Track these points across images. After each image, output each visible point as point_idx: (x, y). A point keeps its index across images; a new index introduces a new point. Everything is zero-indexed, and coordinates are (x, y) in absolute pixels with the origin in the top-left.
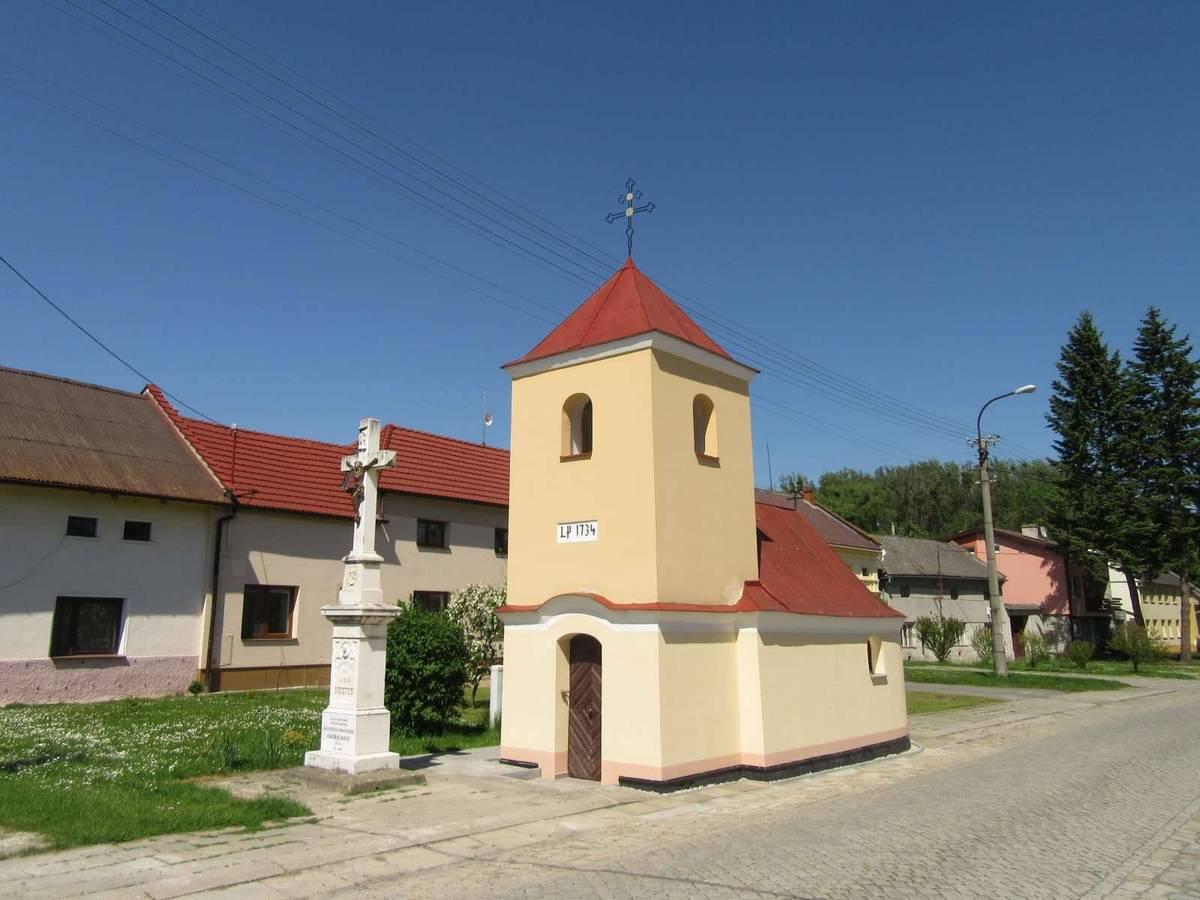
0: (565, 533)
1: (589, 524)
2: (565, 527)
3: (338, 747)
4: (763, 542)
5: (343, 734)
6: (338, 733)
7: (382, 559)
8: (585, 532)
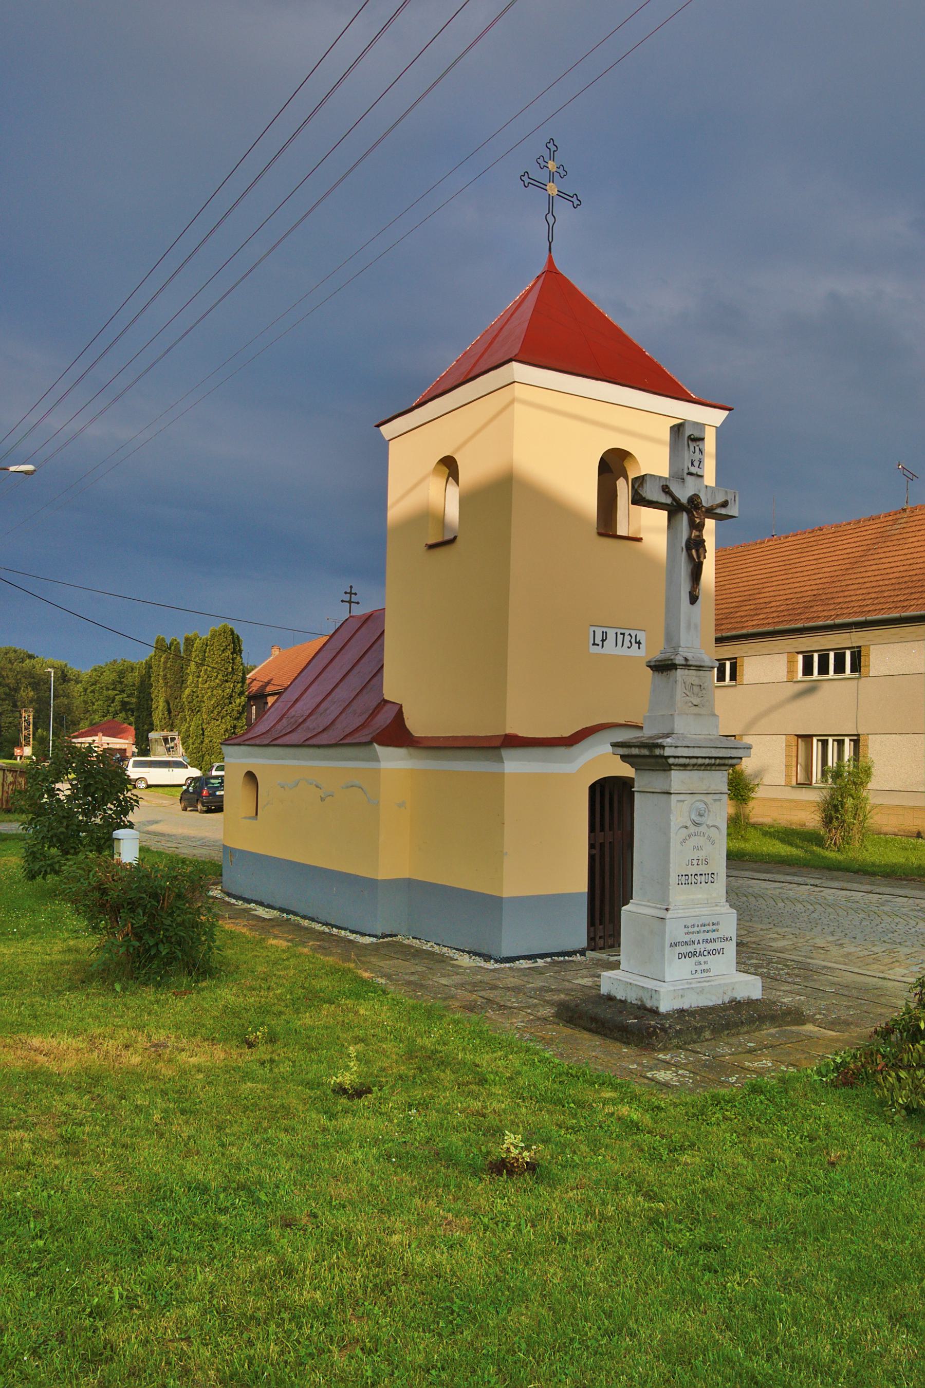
0: (598, 641)
3: (699, 968)
5: (710, 946)
6: (699, 948)
8: (627, 643)
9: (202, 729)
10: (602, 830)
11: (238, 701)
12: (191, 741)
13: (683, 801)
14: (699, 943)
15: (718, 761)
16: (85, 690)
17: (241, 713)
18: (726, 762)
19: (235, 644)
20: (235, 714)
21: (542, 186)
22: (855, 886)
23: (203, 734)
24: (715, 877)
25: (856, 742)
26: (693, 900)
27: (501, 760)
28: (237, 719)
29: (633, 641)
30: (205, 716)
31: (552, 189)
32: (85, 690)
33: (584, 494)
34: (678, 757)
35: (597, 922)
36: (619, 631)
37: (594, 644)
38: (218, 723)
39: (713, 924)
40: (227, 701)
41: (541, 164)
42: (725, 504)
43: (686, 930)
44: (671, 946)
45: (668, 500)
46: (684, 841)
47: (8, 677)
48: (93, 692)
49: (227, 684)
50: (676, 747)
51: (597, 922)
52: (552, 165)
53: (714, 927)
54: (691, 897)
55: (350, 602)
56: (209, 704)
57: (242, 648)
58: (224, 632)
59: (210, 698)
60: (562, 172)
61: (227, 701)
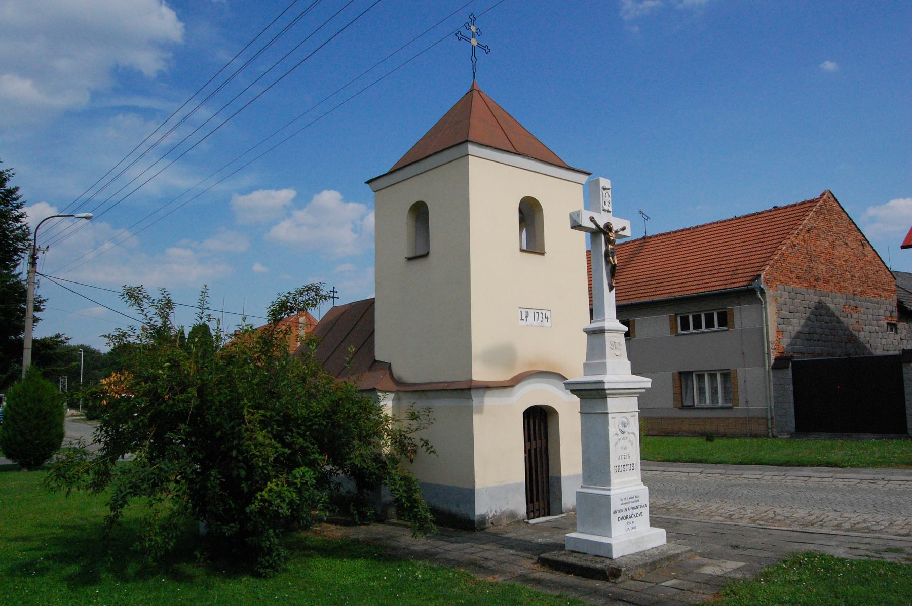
0: (524, 318)
2: (524, 311)
3: (630, 526)
5: (635, 512)
6: (629, 513)
8: (540, 319)
10: (535, 440)
22: (670, 469)
25: (726, 375)
27: (470, 398)
31: (474, 42)
41: (467, 26)
42: (624, 229)
45: (594, 227)
52: (473, 29)
55: (333, 297)
60: (479, 33)
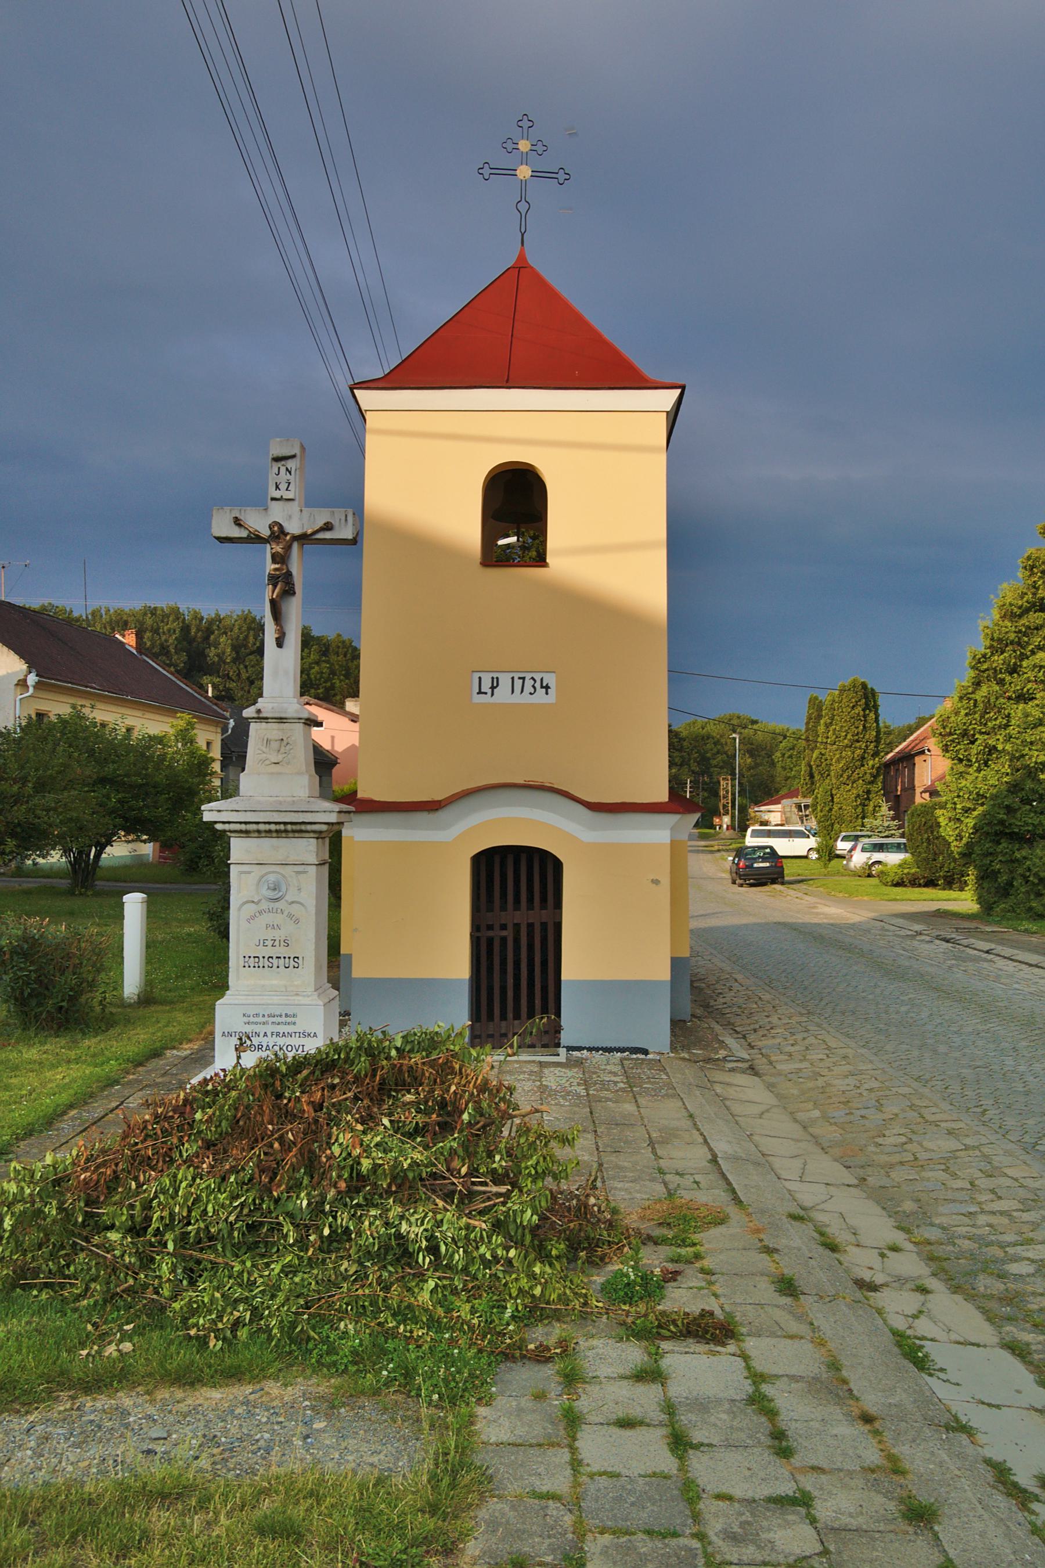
0: (486, 687)
1: (538, 678)
4: (821, 1548)
7: (354, 809)
8: (528, 687)
9: (832, 795)
11: (871, 763)
12: (819, 808)
13: (249, 873)
14: (265, 1035)
15: (289, 827)
16: (783, 755)
17: (875, 777)
18: (303, 827)
19: (868, 698)
20: (868, 777)
21: (511, 172)
23: (832, 800)
24: (300, 961)
26: (263, 986)
28: (872, 783)
29: (538, 685)
30: (834, 781)
31: (524, 172)
32: (783, 755)
33: (463, 522)
34: (229, 823)
35: (510, 1015)
36: (516, 676)
37: (480, 692)
38: (849, 787)
39: (286, 1015)
40: (858, 763)
42: (328, 527)
43: (246, 1019)
44: (224, 1034)
46: (253, 917)
47: (726, 744)
48: (790, 757)
49: (858, 745)
50: (219, 811)
51: (510, 1015)
53: (289, 1020)
54: (262, 982)
56: (836, 767)
57: (879, 703)
58: (854, 687)
59: (838, 761)
61: (858, 763)
